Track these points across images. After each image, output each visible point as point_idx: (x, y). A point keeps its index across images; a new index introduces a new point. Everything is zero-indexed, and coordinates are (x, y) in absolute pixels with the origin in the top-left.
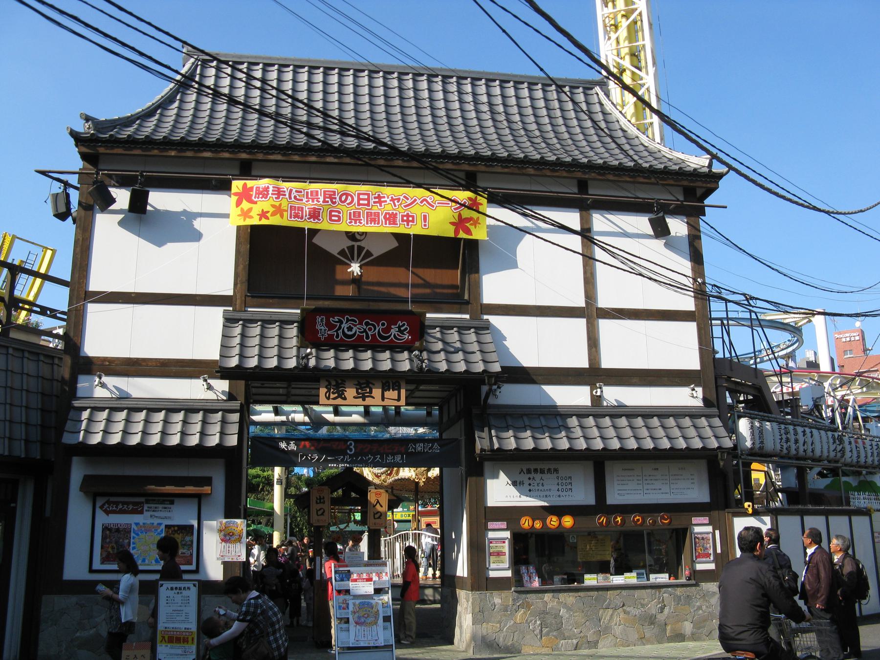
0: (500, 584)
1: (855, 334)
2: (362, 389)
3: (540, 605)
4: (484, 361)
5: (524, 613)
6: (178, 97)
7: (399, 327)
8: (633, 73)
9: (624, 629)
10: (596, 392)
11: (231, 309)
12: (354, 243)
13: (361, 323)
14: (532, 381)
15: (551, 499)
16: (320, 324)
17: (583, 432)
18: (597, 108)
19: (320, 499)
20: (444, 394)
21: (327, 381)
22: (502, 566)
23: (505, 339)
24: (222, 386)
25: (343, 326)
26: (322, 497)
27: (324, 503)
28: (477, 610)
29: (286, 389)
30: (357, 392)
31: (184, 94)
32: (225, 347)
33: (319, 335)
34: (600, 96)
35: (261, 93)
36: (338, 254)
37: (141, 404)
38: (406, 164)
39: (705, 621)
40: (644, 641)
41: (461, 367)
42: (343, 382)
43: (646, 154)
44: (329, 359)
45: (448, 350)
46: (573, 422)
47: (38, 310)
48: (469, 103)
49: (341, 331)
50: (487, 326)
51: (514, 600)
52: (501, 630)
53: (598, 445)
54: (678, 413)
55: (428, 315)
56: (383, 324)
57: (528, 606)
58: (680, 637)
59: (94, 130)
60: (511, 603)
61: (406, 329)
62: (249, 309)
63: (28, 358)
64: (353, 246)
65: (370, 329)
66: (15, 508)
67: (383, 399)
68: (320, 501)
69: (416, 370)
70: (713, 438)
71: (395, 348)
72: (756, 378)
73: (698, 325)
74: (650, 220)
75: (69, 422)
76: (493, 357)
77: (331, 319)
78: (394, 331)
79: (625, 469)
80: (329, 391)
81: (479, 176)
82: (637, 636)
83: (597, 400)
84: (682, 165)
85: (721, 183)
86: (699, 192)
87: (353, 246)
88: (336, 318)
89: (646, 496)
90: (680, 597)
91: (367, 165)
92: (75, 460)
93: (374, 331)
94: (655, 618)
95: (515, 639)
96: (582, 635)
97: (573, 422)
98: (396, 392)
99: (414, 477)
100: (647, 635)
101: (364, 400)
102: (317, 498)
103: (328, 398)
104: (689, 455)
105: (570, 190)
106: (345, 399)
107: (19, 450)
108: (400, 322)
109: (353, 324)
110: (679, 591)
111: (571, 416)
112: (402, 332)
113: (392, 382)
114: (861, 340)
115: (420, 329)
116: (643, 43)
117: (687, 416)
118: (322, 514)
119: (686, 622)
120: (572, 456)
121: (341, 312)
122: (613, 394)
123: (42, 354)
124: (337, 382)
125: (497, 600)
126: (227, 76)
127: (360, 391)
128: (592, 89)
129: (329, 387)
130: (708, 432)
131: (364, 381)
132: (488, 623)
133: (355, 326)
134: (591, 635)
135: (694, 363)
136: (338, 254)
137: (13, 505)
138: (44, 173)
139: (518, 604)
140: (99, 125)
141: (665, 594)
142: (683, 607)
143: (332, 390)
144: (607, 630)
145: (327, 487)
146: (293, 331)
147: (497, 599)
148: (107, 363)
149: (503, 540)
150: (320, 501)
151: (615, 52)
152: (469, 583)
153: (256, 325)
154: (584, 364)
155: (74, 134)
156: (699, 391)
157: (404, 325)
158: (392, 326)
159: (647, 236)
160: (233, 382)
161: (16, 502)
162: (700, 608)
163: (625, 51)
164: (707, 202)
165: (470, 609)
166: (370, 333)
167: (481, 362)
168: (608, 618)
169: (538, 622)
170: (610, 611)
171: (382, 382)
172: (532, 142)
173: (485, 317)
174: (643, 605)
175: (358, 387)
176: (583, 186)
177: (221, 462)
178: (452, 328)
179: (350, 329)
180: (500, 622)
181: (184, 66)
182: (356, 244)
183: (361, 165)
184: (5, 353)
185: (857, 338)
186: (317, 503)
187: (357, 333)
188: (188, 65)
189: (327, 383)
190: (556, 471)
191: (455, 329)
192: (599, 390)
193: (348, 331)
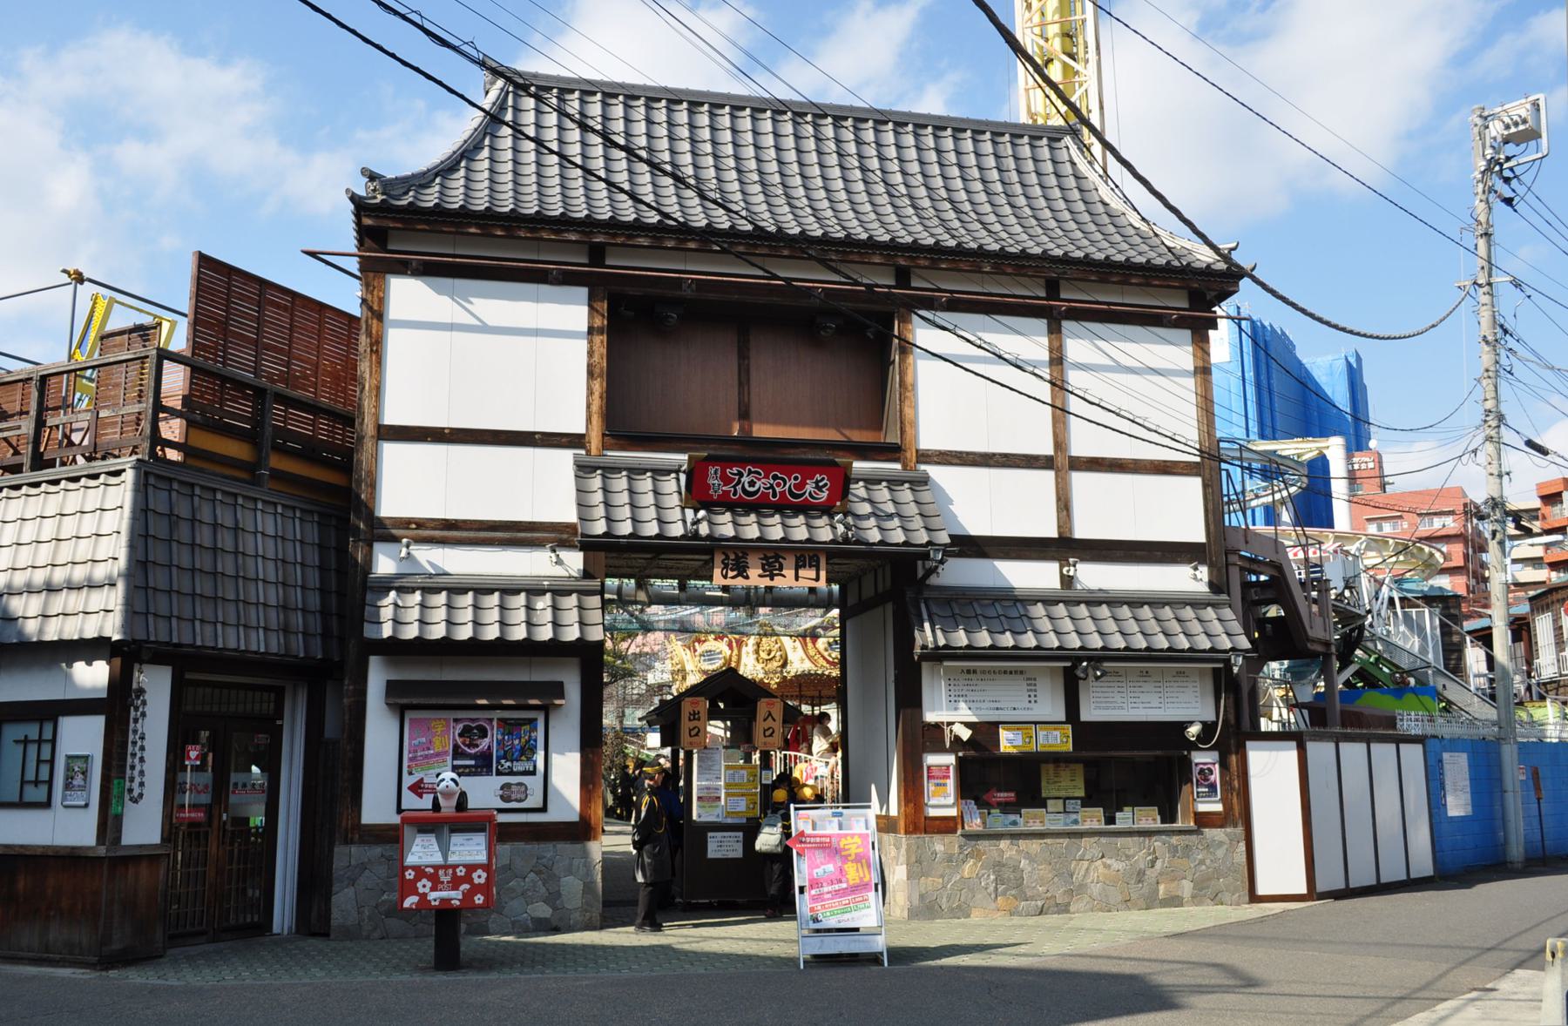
0: (945, 826)
1: (1368, 459)
2: (770, 564)
3: (995, 854)
4: (928, 529)
5: (975, 864)
6: (487, 142)
7: (817, 482)
8: (1065, 65)
9: (1104, 889)
10: (1068, 571)
11: (583, 452)
13: (766, 477)
14: (982, 554)
15: (983, 712)
17: (1053, 624)
18: (1067, 169)
19: (694, 714)
21: (724, 553)
22: (942, 801)
23: (951, 501)
24: (574, 561)
25: (743, 480)
27: (699, 719)
28: (913, 859)
31: (494, 136)
32: (582, 505)
33: (711, 492)
34: (1071, 151)
35: (537, 104)
37: (489, 583)
39: (1209, 879)
40: (1129, 904)
41: (898, 537)
42: (745, 555)
43: (1138, 240)
44: (725, 526)
45: (880, 516)
46: (1039, 610)
48: (891, 160)
49: (740, 486)
50: (925, 480)
51: (960, 847)
52: (944, 887)
53: (1074, 642)
54: (1176, 601)
56: (796, 478)
57: (977, 855)
58: (1174, 901)
59: (383, 194)
60: (956, 850)
61: (826, 485)
63: (154, 486)
65: (778, 485)
66: (282, 725)
67: (797, 578)
69: (840, 539)
70: (1224, 636)
71: (806, 509)
72: (1277, 552)
73: (1203, 481)
76: (935, 522)
82: (1120, 898)
83: (1067, 581)
84: (1190, 258)
88: (735, 470)
89: (1132, 712)
90: (1177, 847)
94: (1144, 874)
95: (962, 899)
96: (1049, 895)
97: (1039, 610)
99: (761, 675)
100: (1134, 896)
101: (772, 579)
103: (725, 577)
104: (1193, 655)
105: (1035, 291)
106: (747, 577)
107: (298, 647)
110: (1174, 840)
111: (1035, 602)
112: (820, 489)
114: (1377, 468)
115: (843, 483)
116: (1083, 17)
117: (1187, 604)
118: (697, 735)
119: (1184, 881)
120: (1040, 654)
121: (742, 462)
122: (1093, 576)
123: (198, 484)
124: (736, 555)
125: (939, 847)
126: (551, 110)
128: (1059, 140)
130: (1217, 627)
131: (772, 554)
132: (927, 877)
133: (759, 479)
134: (1059, 894)
135: (1197, 534)
137: (279, 722)
139: (966, 852)
140: (388, 185)
141: (1157, 843)
142: (1180, 860)
144: (1082, 887)
146: (670, 485)
147: (939, 845)
148: (414, 526)
151: (1037, 30)
152: (902, 824)
153: (619, 476)
154: (1053, 533)
155: (354, 198)
156: (1203, 572)
157: (823, 479)
159: (1191, 391)
160: (591, 553)
161: (282, 719)
162: (1202, 862)
163: (1053, 30)
165: (902, 858)
166: (778, 490)
167: (923, 530)
168: (1082, 873)
169: (992, 877)
170: (1086, 864)
172: (990, 231)
173: (923, 467)
174: (1128, 857)
176: (1053, 289)
177: (576, 661)
178: (879, 482)
179: (752, 484)
180: (942, 876)
181: (487, 93)
184: (190, 493)
185: (1371, 465)
188: (494, 94)
189: (723, 557)
191: (884, 484)
192: (1072, 569)
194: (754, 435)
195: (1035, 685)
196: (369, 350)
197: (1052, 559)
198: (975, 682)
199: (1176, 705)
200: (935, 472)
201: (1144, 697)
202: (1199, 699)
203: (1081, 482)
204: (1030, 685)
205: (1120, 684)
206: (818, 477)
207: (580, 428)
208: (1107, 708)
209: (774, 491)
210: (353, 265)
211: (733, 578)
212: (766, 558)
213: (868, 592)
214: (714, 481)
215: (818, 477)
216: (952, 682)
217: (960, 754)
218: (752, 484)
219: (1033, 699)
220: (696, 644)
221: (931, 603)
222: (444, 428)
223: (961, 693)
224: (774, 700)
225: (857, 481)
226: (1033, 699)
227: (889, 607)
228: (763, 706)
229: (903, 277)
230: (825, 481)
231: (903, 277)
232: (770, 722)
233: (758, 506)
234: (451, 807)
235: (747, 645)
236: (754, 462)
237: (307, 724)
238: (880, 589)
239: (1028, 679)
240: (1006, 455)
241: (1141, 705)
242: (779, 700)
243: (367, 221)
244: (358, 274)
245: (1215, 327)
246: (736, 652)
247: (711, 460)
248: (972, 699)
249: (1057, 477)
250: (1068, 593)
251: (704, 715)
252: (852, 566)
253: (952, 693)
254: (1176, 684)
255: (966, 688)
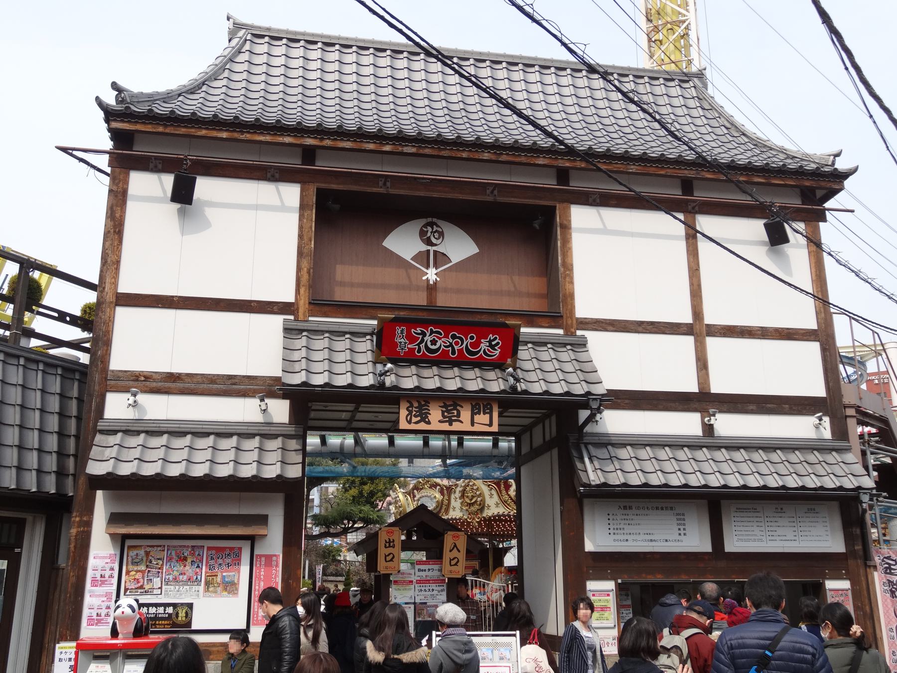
2: (448, 411)
7: (490, 341)
11: (292, 317)
12: (429, 248)
13: (446, 336)
16: (400, 336)
19: (390, 542)
20: (526, 422)
21: (408, 401)
22: (605, 624)
25: (426, 339)
26: (392, 540)
27: (394, 547)
29: (351, 413)
30: (443, 416)
33: (398, 349)
36: (411, 259)
38: (435, 153)
42: (427, 402)
44: (409, 379)
47: (56, 315)
49: (424, 344)
50: (582, 344)
55: (523, 330)
56: (472, 338)
61: (498, 343)
62: (311, 319)
64: (428, 251)
65: (457, 343)
66: (20, 554)
67: (473, 424)
68: (390, 545)
71: (481, 364)
73: (821, 345)
74: (765, 225)
75: (94, 447)
77: (413, 330)
78: (484, 345)
79: (739, 509)
80: (410, 413)
81: (572, 173)
83: (709, 429)
85: (847, 183)
86: (819, 194)
87: (428, 251)
88: (419, 330)
91: (729, 181)
92: (99, 494)
93: (467, 343)
98: (488, 416)
101: (451, 425)
102: (386, 541)
103: (410, 422)
106: (429, 423)
107: (31, 483)
108: (491, 335)
109: (437, 337)
112: (493, 347)
113: (483, 404)
115: (512, 344)
121: (425, 323)
127: (446, 414)
129: (411, 409)
133: (440, 339)
135: (819, 390)
136: (411, 259)
138: (64, 150)
143: (414, 413)
145: (397, 529)
146: (366, 346)
148: (143, 379)
149: (607, 593)
150: (390, 545)
154: (694, 389)
157: (496, 338)
158: (482, 340)
161: (21, 547)
164: (827, 205)
166: (456, 348)
171: (471, 404)
173: (579, 333)
175: (444, 409)
176: (687, 186)
179: (434, 342)
182: (432, 249)
183: (593, 170)
186: (386, 547)
187: (442, 347)
190: (671, 509)
193: (432, 345)
194: (439, 304)
195: (684, 520)
196: (112, 231)
197: (695, 410)
198: (630, 517)
199: (809, 538)
200: (593, 338)
201: (780, 531)
202: (829, 533)
203: (713, 344)
204: (680, 519)
205: (758, 519)
206: (491, 337)
207: (291, 299)
208: (748, 540)
209: (453, 349)
210: (103, 161)
211: (416, 423)
212: (445, 406)
213: (538, 441)
214: (400, 340)
215: (491, 337)
216: (611, 517)
217: (620, 581)
218: (434, 342)
219: (683, 532)
220: (415, 491)
221: (590, 447)
222: (173, 297)
223: (618, 527)
224: (459, 533)
225: (526, 343)
226: (682, 532)
227: (555, 452)
228: (449, 539)
229: (563, 176)
230: (497, 341)
231: (563, 176)
232: (455, 553)
233: (442, 361)
234: (130, 633)
235: (455, 492)
236: (436, 323)
237: (43, 552)
238: (548, 438)
239: (678, 514)
240: (652, 323)
241: (778, 538)
242: (463, 533)
243: (114, 125)
244: (108, 170)
245: (824, 220)
246: (446, 497)
247: (398, 321)
248: (628, 532)
249: (696, 341)
250: (709, 441)
251: (398, 545)
252: (520, 418)
253: (611, 527)
254: (808, 519)
255: (623, 522)
